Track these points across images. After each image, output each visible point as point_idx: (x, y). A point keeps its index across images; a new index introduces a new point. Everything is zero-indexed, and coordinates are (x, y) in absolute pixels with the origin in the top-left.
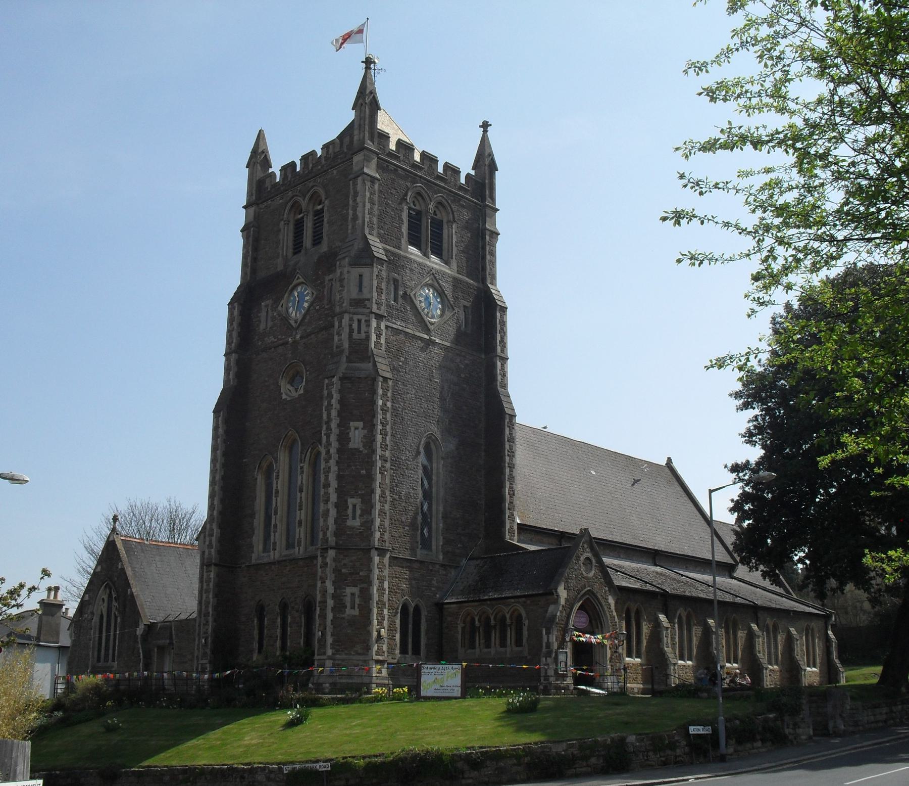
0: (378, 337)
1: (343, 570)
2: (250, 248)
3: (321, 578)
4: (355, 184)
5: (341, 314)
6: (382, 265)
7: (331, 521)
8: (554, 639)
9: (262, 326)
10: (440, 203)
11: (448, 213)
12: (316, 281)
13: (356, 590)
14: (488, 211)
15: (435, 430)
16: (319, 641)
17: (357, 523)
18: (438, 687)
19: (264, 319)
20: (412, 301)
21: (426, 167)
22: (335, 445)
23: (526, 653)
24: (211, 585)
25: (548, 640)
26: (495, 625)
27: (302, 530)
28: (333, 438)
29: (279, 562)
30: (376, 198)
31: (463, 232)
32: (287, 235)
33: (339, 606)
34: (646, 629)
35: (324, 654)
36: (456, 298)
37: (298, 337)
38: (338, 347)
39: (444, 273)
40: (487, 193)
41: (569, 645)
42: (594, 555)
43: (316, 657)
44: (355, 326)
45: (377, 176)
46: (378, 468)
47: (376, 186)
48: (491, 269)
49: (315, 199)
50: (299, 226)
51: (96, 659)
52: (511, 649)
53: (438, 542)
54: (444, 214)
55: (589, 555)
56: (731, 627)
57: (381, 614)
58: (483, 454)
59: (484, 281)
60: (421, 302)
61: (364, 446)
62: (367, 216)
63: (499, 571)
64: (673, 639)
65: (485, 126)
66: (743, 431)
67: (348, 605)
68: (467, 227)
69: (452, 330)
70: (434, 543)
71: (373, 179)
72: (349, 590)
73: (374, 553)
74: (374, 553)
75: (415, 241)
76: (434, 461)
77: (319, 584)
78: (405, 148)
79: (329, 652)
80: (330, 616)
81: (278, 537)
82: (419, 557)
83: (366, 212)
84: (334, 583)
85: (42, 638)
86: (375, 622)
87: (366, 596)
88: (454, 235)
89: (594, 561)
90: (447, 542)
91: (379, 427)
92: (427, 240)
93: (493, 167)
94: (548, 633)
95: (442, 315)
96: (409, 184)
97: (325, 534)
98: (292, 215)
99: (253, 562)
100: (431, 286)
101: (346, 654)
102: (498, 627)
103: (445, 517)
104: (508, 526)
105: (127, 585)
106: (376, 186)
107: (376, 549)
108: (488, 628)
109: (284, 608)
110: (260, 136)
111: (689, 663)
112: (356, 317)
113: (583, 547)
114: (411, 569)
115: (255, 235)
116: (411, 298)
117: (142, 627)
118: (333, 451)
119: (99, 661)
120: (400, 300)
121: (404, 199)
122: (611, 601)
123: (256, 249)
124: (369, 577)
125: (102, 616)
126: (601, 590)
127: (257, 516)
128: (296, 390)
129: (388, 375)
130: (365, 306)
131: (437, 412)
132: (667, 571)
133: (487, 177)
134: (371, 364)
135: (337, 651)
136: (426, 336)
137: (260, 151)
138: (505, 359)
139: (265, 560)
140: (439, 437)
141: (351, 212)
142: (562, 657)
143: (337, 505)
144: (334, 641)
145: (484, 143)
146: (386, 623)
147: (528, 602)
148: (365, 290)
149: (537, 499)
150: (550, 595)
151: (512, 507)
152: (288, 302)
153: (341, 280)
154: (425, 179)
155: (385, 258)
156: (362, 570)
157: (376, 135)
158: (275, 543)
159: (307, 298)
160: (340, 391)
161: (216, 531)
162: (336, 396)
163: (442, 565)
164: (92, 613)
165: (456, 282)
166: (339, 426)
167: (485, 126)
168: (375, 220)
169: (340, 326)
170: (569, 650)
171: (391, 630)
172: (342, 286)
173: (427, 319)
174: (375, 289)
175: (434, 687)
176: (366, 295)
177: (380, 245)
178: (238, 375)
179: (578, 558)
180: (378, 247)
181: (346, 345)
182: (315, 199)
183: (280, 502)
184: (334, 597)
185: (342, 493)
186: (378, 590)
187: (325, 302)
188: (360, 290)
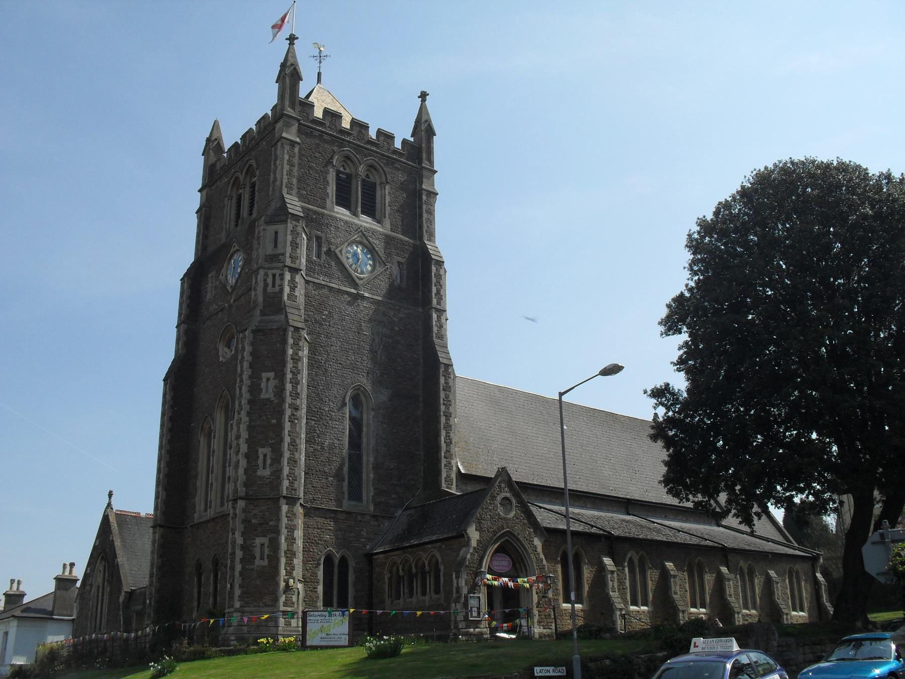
0: (296, 293)
1: (254, 521)
4: (276, 149)
6: (298, 221)
7: (241, 471)
8: (463, 583)
9: (209, 296)
10: (371, 166)
13: (265, 540)
14: (425, 173)
15: (366, 383)
17: (267, 473)
18: (324, 635)
19: (210, 291)
20: (338, 259)
21: (355, 133)
22: (246, 396)
26: (417, 573)
29: (213, 519)
30: (296, 160)
31: (398, 193)
32: (229, 211)
33: (249, 558)
34: (587, 573)
35: (232, 606)
36: (389, 255)
39: (374, 232)
40: (424, 156)
41: (484, 590)
42: (514, 495)
43: (227, 611)
44: (270, 280)
45: (298, 140)
46: (287, 417)
47: (296, 150)
48: (428, 227)
49: (250, 172)
53: (368, 491)
54: (377, 177)
55: (508, 495)
56: (695, 572)
58: (421, 405)
59: (421, 238)
60: (348, 258)
61: (275, 396)
62: (285, 177)
64: (621, 583)
66: (675, 360)
67: (258, 555)
68: (402, 187)
69: (384, 286)
70: (364, 494)
71: (293, 144)
72: (258, 541)
73: (283, 501)
74: (283, 501)
75: (344, 200)
76: (365, 412)
78: (332, 116)
79: (237, 605)
80: (238, 567)
81: (214, 496)
82: (345, 508)
83: (285, 173)
84: (243, 534)
85: (55, 612)
86: (283, 572)
87: (274, 545)
88: (387, 196)
89: (514, 501)
91: (289, 376)
92: (357, 201)
93: (431, 132)
94: (457, 578)
95: (373, 270)
96: (335, 149)
98: (235, 191)
99: (196, 521)
100: (361, 243)
101: (255, 606)
103: (377, 467)
104: (444, 475)
105: (115, 556)
106: (296, 150)
107: (284, 497)
108: (411, 577)
110: (216, 126)
111: (645, 608)
112: (270, 272)
113: (500, 487)
114: (336, 520)
116: (336, 254)
117: (123, 594)
120: (324, 257)
121: (329, 162)
122: (537, 542)
124: (278, 526)
126: (523, 532)
127: (199, 476)
129: (299, 325)
130: (279, 261)
131: (367, 363)
132: (638, 519)
133: (424, 141)
134: (283, 316)
135: (247, 603)
136: (353, 291)
137: (213, 138)
138: (441, 311)
140: (368, 387)
142: (473, 603)
143: (247, 456)
144: (243, 593)
145: (423, 110)
148: (279, 246)
149: (473, 447)
150: (461, 537)
151: (449, 455)
152: (227, 269)
154: (354, 144)
155: (301, 214)
157: (297, 103)
163: (374, 516)
165: (388, 240)
166: (250, 377)
167: (423, 96)
168: (295, 181)
169: (256, 282)
170: (483, 595)
172: (259, 244)
173: (355, 274)
174: (288, 244)
175: (320, 635)
176: (280, 250)
177: (299, 204)
179: (493, 498)
180: (294, 205)
181: (260, 299)
183: (216, 461)
184: (243, 547)
185: (253, 444)
186: (286, 539)
188: (276, 246)
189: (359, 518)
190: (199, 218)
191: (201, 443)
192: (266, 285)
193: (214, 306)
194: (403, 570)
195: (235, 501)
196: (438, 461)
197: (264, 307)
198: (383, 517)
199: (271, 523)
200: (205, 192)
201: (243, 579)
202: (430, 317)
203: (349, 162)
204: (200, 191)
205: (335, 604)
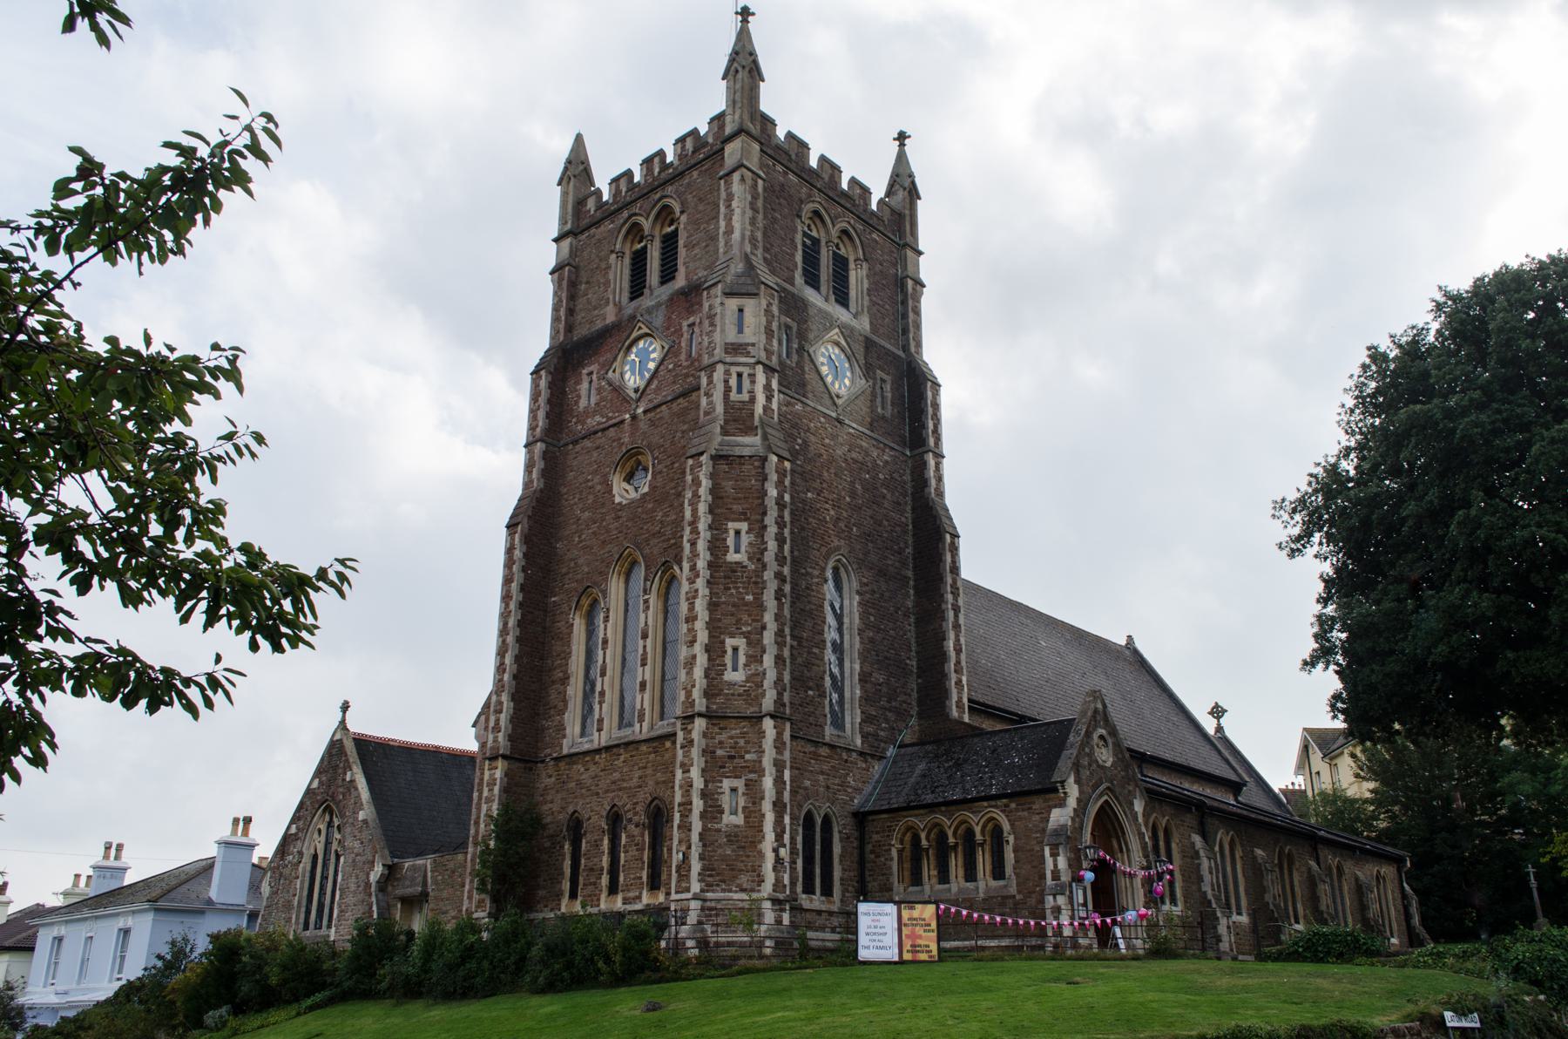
2: (564, 295)
3: (683, 765)
4: (729, 185)
5: (711, 368)
7: (698, 673)
9: (583, 403)
11: (855, 247)
12: (670, 332)
13: (739, 784)
14: (909, 253)
16: (679, 868)
19: (586, 393)
23: (1013, 890)
24: (496, 789)
25: (1055, 865)
27: (647, 696)
28: (701, 546)
29: (608, 748)
32: (620, 272)
33: (712, 811)
35: (688, 890)
37: (640, 410)
38: (707, 414)
44: (733, 382)
50: (639, 260)
51: (301, 926)
52: (985, 883)
57: (779, 822)
61: (750, 559)
63: (978, 754)
65: (902, 137)
70: (848, 719)
72: (727, 784)
77: (679, 774)
79: (696, 887)
80: (697, 826)
81: (607, 710)
90: (867, 719)
93: (913, 194)
97: (689, 694)
99: (565, 751)
101: (724, 891)
102: (960, 848)
103: (864, 678)
104: (955, 698)
109: (615, 820)
110: (579, 139)
112: (734, 370)
115: (571, 279)
118: (701, 564)
119: (306, 927)
123: (572, 297)
125: (315, 857)
127: (572, 680)
128: (636, 489)
130: (748, 354)
138: (939, 456)
139: (587, 747)
141: (722, 224)
143: (708, 649)
144: (704, 869)
145: (901, 158)
146: (787, 837)
147: (1013, 805)
152: (623, 363)
153: (711, 317)
156: (748, 752)
158: (601, 721)
159: (653, 356)
160: (712, 476)
161: (507, 704)
162: (706, 483)
163: (861, 754)
164: (301, 853)
166: (710, 527)
167: (902, 137)
169: (710, 382)
171: (793, 852)
172: (712, 324)
178: (544, 473)
181: (720, 409)
182: (665, 214)
187: (683, 357)
188: (740, 331)
189: (845, 756)
190: (558, 285)
191: (575, 628)
192: (728, 389)
193: (598, 418)
194: (928, 838)
195: (689, 719)
196: (944, 676)
197: (726, 422)
198: (873, 756)
199: (748, 757)
200: (566, 243)
201: (704, 845)
202: (925, 464)
203: (818, 222)
204: (556, 240)
205: (818, 891)
